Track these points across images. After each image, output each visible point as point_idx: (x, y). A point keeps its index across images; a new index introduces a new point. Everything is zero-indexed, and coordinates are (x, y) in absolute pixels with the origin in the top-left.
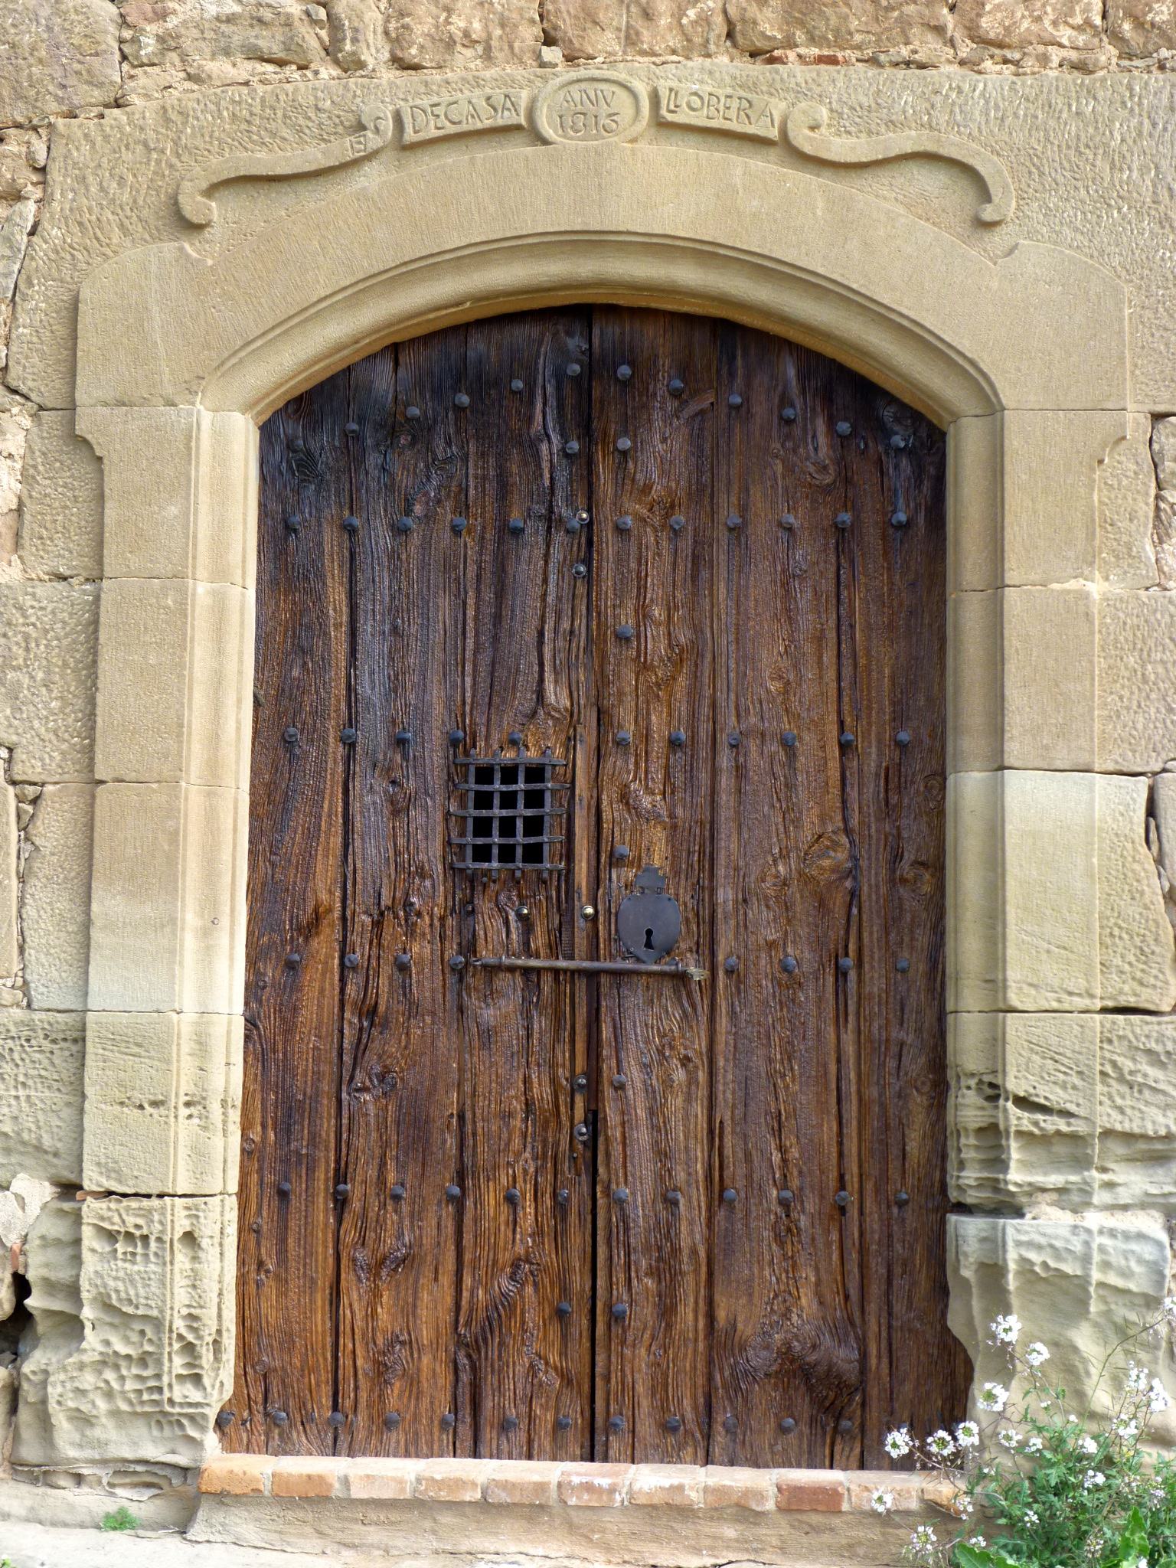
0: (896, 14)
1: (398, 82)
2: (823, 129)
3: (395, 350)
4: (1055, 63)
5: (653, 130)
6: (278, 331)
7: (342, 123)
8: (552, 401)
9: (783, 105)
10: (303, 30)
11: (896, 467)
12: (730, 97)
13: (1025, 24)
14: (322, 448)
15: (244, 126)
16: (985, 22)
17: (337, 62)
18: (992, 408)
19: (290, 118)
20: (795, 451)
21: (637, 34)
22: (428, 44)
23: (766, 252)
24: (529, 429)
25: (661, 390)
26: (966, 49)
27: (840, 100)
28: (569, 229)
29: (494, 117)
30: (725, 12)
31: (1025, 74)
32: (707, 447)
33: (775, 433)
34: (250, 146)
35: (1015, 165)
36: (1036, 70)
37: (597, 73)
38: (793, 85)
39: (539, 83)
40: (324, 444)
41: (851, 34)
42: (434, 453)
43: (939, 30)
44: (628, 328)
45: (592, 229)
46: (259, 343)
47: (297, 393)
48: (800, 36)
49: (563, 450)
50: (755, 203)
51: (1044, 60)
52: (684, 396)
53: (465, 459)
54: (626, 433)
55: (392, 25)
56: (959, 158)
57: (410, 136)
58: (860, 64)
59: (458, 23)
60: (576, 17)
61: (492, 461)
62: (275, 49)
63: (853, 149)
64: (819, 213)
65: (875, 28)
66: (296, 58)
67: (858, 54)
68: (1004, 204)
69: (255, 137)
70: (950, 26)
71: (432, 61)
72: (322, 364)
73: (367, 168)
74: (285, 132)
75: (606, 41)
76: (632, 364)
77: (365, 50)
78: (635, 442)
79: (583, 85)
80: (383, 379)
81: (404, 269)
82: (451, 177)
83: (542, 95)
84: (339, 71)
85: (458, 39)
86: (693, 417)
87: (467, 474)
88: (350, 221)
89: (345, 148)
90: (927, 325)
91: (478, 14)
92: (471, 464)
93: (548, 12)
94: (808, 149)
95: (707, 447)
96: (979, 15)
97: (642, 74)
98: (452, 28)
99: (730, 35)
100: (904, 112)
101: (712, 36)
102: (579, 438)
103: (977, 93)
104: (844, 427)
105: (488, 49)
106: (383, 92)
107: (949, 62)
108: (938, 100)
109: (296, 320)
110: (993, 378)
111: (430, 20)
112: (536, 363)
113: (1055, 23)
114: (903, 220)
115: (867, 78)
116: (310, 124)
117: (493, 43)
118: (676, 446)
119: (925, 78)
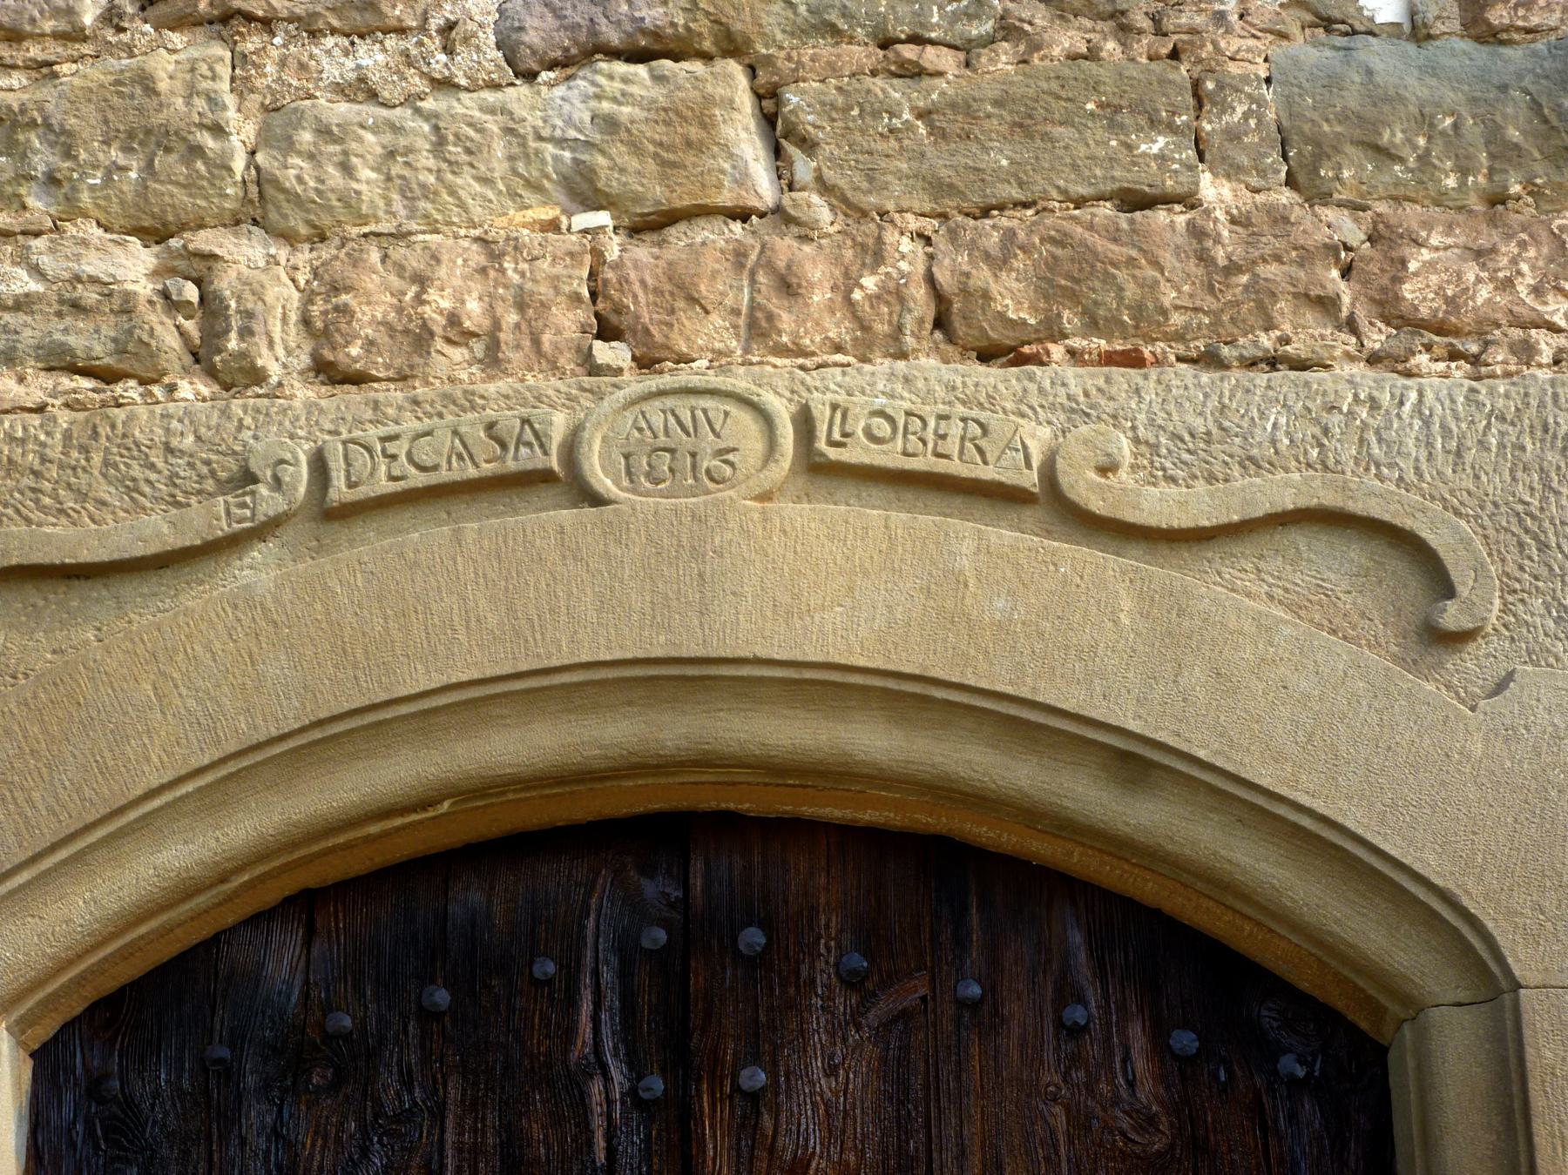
0: (1244, 279)
1: (323, 403)
2: (1123, 474)
3: (305, 907)
4: (1546, 356)
5: (801, 481)
6: (63, 854)
7: (213, 473)
8: (612, 999)
9: (1045, 432)
10: (153, 318)
11: (1292, 1117)
12: (946, 417)
13: (1484, 293)
14: (156, 1094)
15: (28, 481)
16: (1408, 291)
17: (212, 373)
18: (1492, 986)
19: (116, 466)
20: (1090, 1089)
21: (770, 317)
22: (382, 338)
23: (1025, 693)
24: (566, 1051)
25: (824, 972)
26: (1377, 337)
27: (1152, 422)
28: (641, 654)
29: (502, 459)
30: (930, 279)
31: (1493, 376)
32: (917, 1083)
33: (1049, 1055)
34: (36, 516)
35: (1491, 532)
36: (1513, 368)
37: (695, 381)
38: (1063, 399)
39: (586, 401)
40: (160, 1085)
41: (1164, 312)
42: (377, 1101)
43: (1326, 304)
44: (757, 859)
45: (685, 653)
46: (24, 876)
47: (109, 985)
48: (1069, 318)
49: (633, 1092)
50: (1000, 604)
51: (1526, 352)
52: (870, 986)
53: (439, 1114)
54: (756, 1059)
55: (316, 310)
56: (1387, 517)
57: (339, 490)
58: (1184, 366)
59: (439, 301)
60: (657, 291)
61: (492, 1118)
62: (98, 349)
63: (1182, 504)
64: (1125, 620)
65: (1209, 302)
66: (138, 368)
67: (1181, 349)
68: (1477, 599)
69: (47, 501)
70: (1346, 299)
71: (388, 367)
72: (154, 924)
73: (256, 554)
74: (105, 491)
75: (712, 331)
76: (766, 925)
77: (265, 351)
78: (773, 1076)
79: (669, 402)
80: (282, 963)
81: (317, 734)
82: (416, 564)
83: (593, 418)
84: (216, 388)
85: (438, 330)
86: (887, 1025)
87: (442, 1141)
88: (217, 646)
89: (215, 516)
90: (1350, 824)
91: (477, 287)
92: (450, 1123)
93: (606, 282)
94: (1097, 505)
95: (917, 1083)
96: (1398, 280)
97: (781, 384)
98: (427, 310)
99: (941, 323)
100: (1274, 442)
101: (909, 323)
102: (663, 1071)
103: (1407, 407)
104: (1185, 1041)
105: (494, 346)
106: (294, 423)
107: (1350, 357)
108: (1335, 420)
109: (100, 833)
110: (1490, 925)
111: (388, 298)
112: (582, 927)
113: (1537, 291)
114: (1287, 631)
115: (1199, 386)
116: (153, 476)
117: (502, 336)
118: (855, 1083)
119: (1307, 384)
